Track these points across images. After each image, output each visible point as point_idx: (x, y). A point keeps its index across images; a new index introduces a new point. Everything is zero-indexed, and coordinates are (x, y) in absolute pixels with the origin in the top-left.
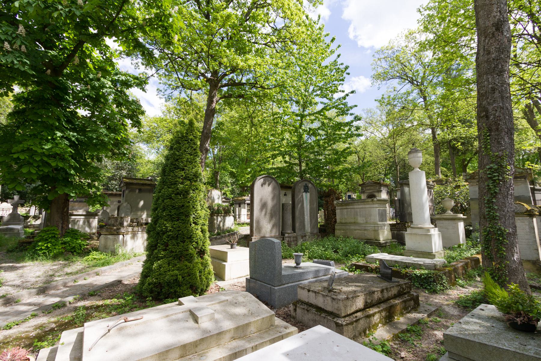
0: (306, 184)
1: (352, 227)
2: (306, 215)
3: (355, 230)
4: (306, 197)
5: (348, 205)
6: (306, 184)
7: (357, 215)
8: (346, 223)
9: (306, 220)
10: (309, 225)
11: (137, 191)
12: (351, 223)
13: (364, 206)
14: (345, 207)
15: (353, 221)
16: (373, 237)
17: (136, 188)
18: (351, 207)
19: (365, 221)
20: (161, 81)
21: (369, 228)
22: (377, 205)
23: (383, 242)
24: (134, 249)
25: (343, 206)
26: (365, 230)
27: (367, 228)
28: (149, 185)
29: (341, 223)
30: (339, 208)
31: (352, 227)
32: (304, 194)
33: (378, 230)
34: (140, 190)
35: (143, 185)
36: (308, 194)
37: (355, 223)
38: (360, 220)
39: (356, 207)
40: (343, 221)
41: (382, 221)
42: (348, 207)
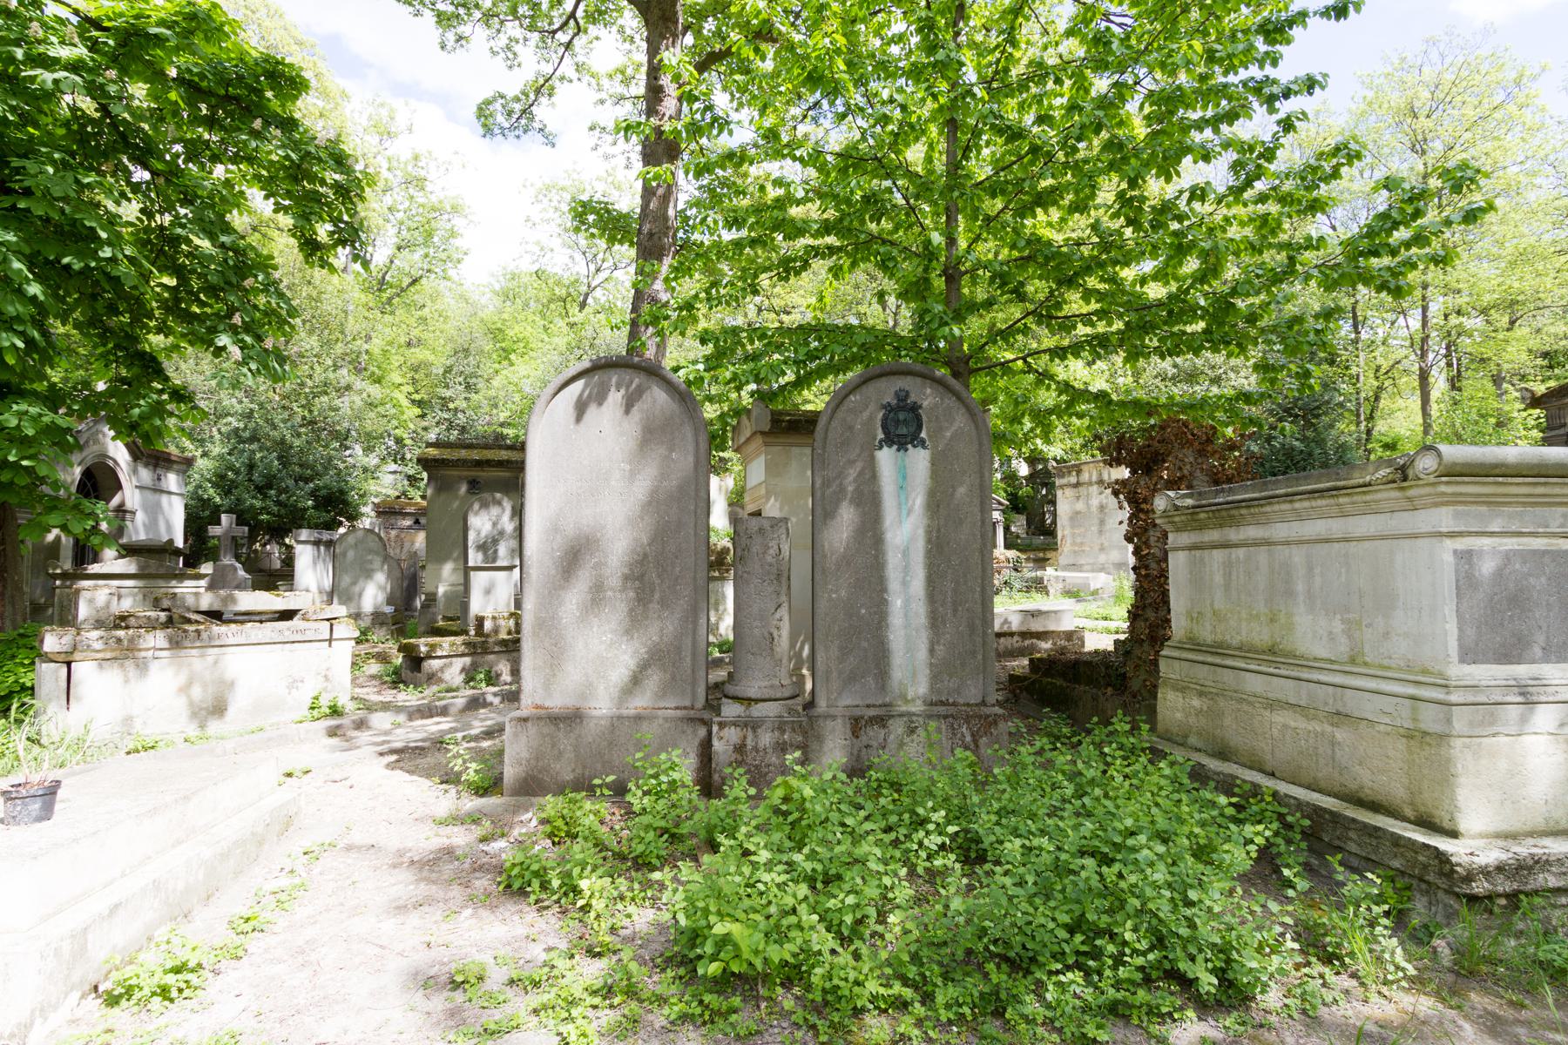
0: (902, 396)
1: (1254, 684)
2: (894, 585)
3: (1273, 704)
4: (903, 474)
5: (1235, 522)
6: (902, 396)
7: (1290, 594)
8: (1218, 649)
9: (896, 619)
10: (922, 654)
11: (463, 489)
12: (1246, 651)
13: (1336, 527)
14: (1213, 535)
15: (1260, 635)
16: (1393, 787)
17: (461, 478)
18: (1251, 532)
19: (1343, 648)
20: (603, 95)
21: (1367, 707)
22: (1444, 518)
23: (1490, 856)
24: (138, 725)
25: (1202, 527)
26: (1340, 717)
27: (1352, 703)
28: (500, 464)
29: (1195, 645)
30: (1185, 538)
31: (1254, 684)
32: (886, 457)
33: (1443, 737)
34: (474, 486)
35: (479, 464)
36: (919, 460)
37: (1274, 655)
38: (1312, 633)
39: (1280, 531)
40: (1206, 634)
41: (1506, 656)
42: (1233, 535)
